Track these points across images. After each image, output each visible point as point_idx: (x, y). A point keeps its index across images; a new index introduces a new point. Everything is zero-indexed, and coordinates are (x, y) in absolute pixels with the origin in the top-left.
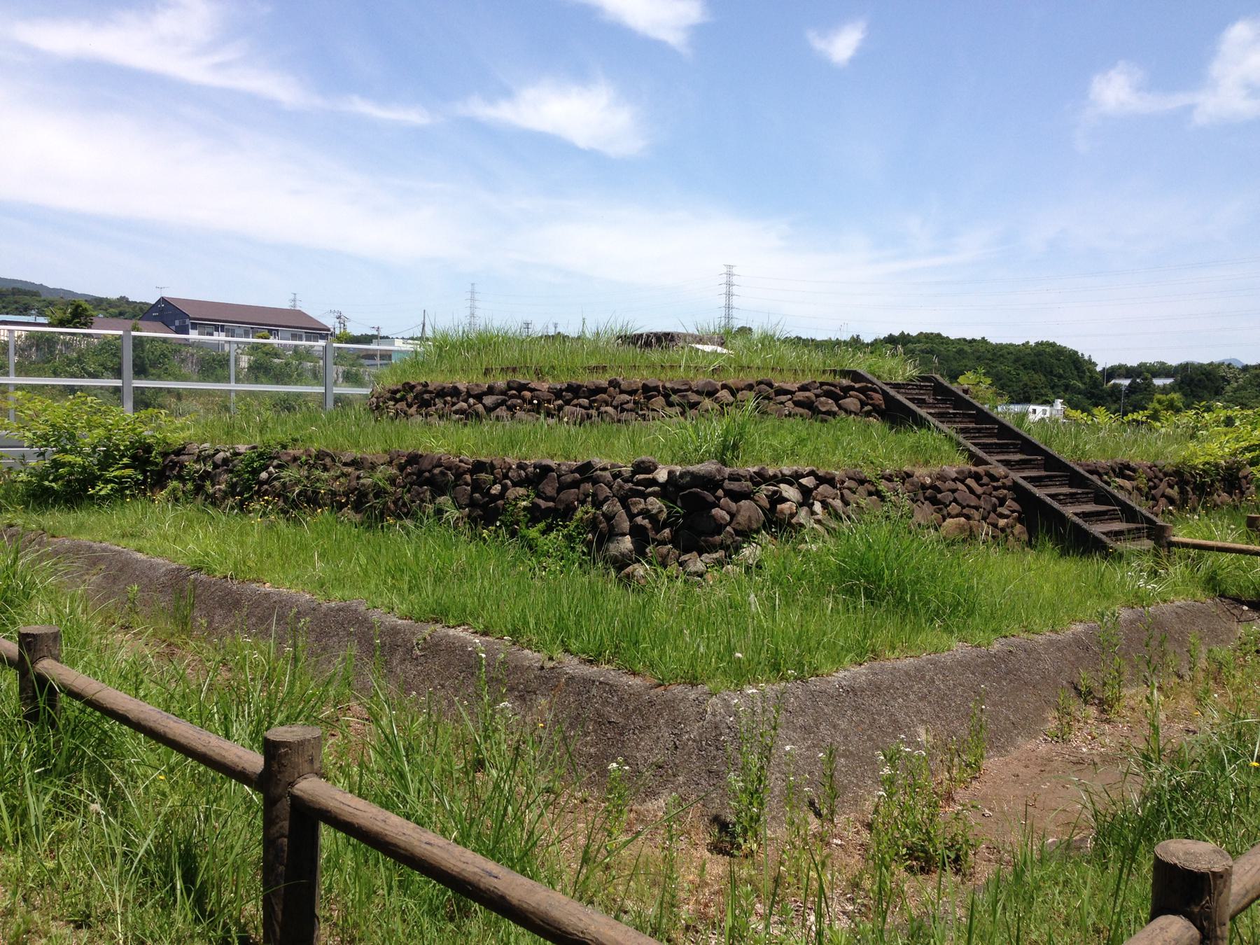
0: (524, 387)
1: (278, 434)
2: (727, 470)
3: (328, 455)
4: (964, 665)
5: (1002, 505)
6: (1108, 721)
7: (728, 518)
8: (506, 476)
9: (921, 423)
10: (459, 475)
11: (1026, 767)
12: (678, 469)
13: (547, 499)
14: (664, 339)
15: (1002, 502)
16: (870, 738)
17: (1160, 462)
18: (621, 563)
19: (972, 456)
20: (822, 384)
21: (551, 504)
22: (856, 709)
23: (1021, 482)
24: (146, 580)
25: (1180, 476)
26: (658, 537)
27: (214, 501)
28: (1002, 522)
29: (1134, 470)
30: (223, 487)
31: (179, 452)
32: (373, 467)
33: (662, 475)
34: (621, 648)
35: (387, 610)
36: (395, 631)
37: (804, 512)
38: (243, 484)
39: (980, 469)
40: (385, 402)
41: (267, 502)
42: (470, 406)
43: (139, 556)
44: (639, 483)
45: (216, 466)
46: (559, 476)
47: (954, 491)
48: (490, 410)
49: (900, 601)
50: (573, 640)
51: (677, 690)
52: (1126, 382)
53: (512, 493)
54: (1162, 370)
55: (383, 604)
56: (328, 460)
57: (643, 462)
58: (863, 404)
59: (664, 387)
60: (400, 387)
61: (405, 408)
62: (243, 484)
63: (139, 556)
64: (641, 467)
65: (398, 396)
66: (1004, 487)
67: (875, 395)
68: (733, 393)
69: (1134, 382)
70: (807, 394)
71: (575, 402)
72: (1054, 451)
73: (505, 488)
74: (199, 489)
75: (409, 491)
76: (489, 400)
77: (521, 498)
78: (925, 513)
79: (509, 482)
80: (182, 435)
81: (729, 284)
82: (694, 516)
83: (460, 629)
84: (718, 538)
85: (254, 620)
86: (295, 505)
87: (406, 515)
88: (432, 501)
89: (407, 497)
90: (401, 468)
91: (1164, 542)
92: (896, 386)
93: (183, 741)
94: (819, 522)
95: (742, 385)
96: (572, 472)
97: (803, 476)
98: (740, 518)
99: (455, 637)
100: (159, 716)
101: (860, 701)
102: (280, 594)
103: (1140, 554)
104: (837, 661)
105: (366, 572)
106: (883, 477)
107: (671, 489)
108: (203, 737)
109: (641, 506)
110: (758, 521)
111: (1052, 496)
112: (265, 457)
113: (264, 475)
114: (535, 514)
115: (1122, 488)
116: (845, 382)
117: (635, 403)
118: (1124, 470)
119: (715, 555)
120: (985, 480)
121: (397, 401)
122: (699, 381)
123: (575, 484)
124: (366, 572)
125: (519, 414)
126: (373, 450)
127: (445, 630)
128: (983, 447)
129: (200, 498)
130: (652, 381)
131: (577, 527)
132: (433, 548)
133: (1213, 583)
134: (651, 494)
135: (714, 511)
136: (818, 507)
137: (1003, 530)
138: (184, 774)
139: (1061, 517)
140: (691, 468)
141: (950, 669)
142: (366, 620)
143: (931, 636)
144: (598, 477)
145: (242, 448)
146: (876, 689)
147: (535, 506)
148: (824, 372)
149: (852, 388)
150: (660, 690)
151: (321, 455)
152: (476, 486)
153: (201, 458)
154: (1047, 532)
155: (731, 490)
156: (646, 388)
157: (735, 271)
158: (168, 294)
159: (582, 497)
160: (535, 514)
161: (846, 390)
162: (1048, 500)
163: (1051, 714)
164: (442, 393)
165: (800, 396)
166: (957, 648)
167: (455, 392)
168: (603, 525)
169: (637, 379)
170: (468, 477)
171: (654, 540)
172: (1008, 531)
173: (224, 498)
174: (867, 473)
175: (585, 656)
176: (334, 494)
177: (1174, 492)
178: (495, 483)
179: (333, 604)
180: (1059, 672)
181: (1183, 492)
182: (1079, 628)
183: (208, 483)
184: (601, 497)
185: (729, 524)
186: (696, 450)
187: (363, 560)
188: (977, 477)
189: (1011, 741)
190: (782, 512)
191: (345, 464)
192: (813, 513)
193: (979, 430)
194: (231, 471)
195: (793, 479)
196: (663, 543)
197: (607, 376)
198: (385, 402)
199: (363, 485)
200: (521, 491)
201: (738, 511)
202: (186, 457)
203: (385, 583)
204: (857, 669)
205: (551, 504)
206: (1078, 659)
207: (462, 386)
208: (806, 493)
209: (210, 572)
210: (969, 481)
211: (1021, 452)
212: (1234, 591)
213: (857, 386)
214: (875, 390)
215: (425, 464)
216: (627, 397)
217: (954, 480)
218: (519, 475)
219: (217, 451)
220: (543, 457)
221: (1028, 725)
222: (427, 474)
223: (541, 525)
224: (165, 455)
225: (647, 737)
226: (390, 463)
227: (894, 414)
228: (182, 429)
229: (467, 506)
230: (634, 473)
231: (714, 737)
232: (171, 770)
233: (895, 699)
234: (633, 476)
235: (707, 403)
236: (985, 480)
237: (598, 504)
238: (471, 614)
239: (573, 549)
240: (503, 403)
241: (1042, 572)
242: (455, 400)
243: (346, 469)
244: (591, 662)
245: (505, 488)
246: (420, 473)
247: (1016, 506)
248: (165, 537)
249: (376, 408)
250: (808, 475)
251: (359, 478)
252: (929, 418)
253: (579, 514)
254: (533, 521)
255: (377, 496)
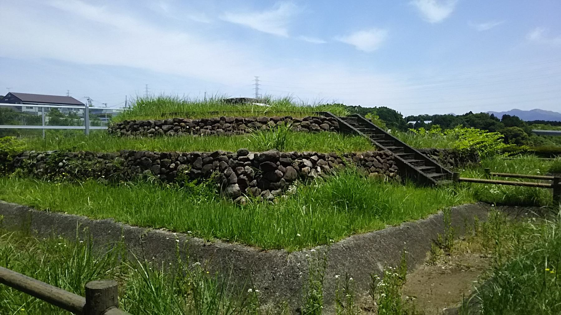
0: (182, 121)
1: (67, 145)
2: (281, 153)
3: (91, 153)
4: (391, 234)
5: (391, 167)
6: (449, 255)
7: (282, 174)
8: (177, 160)
9: (355, 133)
10: (154, 160)
11: (422, 277)
12: (259, 154)
13: (197, 169)
14: (242, 101)
15: (391, 165)
16: (359, 269)
17: (447, 148)
18: (234, 196)
19: (377, 147)
20: (313, 118)
21: (200, 171)
22: (351, 256)
23: (398, 157)
24: (7, 213)
25: (455, 154)
26: (251, 184)
27: (38, 176)
28: (392, 174)
29: (438, 152)
30: (42, 170)
31: (20, 155)
32: (113, 158)
33: (251, 156)
34: (244, 234)
35: (126, 222)
36: (129, 232)
37: (313, 170)
38: (50, 168)
39: (382, 152)
40: (115, 130)
41: (64, 176)
42: (156, 130)
43: (3, 202)
44: (241, 160)
45: (38, 161)
46: (203, 159)
47: (373, 161)
48: (165, 132)
49: (361, 207)
50: (218, 232)
51: (271, 252)
52: (414, 122)
53: (181, 167)
54: (427, 118)
55: (123, 219)
56: (91, 156)
57: (242, 151)
58: (330, 126)
59: (245, 120)
60: (122, 123)
61: (125, 132)
62: (50, 168)
63: (3, 202)
64: (241, 153)
65: (122, 127)
66: (391, 159)
67: (335, 122)
68: (276, 121)
69: (417, 122)
70: (307, 122)
71: (205, 127)
72: (407, 144)
73: (177, 165)
74: (30, 171)
75: (130, 168)
76: (165, 127)
77: (185, 169)
78: (362, 171)
79: (179, 162)
80: (22, 147)
81: (257, 85)
82: (268, 174)
83: (162, 229)
84: (278, 183)
85: (60, 229)
86: (76, 176)
87: (130, 179)
88: (142, 172)
89: (129, 171)
90: (126, 158)
91: (457, 180)
92: (343, 119)
93: (36, 290)
94: (320, 175)
95: (279, 118)
96: (209, 156)
97: (312, 155)
98: (287, 174)
99: (159, 233)
100: (21, 277)
101: (353, 253)
102: (72, 217)
103: (448, 186)
104: (340, 235)
105: (113, 205)
106: (344, 156)
107: (255, 163)
108: (48, 288)
109: (243, 170)
110: (295, 175)
111: (410, 163)
112: (61, 156)
113: (61, 164)
114: (192, 176)
115: (435, 159)
116: (322, 117)
117: (233, 127)
118: (434, 152)
119: (278, 191)
120: (384, 156)
121: (121, 129)
122: (260, 117)
123: (211, 162)
124: (113, 205)
125: (180, 133)
126: (112, 150)
127: (155, 230)
128: (380, 143)
129: (31, 175)
130: (239, 118)
131: (212, 181)
132: (146, 194)
133: (476, 196)
134: (246, 165)
135: (276, 171)
136: (319, 169)
137: (392, 177)
138: (34, 307)
139: (416, 171)
140: (265, 153)
141: (386, 236)
142: (115, 227)
143: (377, 222)
144: (222, 158)
145: (50, 152)
146: (358, 247)
147: (192, 172)
148: (313, 113)
149: (326, 119)
150: (263, 253)
151: (87, 154)
152: (163, 165)
153: (30, 158)
154: (410, 177)
155: (283, 162)
156: (237, 121)
157: (259, 79)
158: (12, 91)
159: (214, 167)
160: (192, 176)
161: (323, 120)
162: (409, 164)
163: (428, 253)
164: (142, 125)
165: (304, 123)
166: (388, 228)
167: (149, 124)
168: (225, 180)
169: (233, 117)
170: (159, 161)
171: (249, 185)
172: (394, 178)
173: (42, 175)
174: (338, 154)
175: (224, 239)
176: (94, 171)
177: (452, 161)
178: (172, 163)
179: (98, 221)
180: (427, 235)
181: (455, 161)
182: (431, 216)
183: (35, 168)
184: (223, 167)
185: (283, 177)
186: (265, 145)
187: (112, 199)
188: (381, 155)
189: (414, 266)
190: (304, 171)
191: (99, 157)
192: (317, 172)
193: (377, 137)
194: (45, 163)
195: (308, 157)
196: (254, 186)
197: (219, 115)
198: (115, 130)
199: (108, 166)
200: (185, 166)
201: (286, 171)
202: (24, 157)
203: (123, 210)
204: (349, 238)
205: (200, 171)
206: (433, 229)
207: (152, 121)
208: (314, 163)
209: (39, 208)
210: (377, 157)
211: (395, 145)
212: (485, 199)
213: (327, 118)
214: (335, 120)
215: (138, 156)
216: (229, 125)
217: (372, 157)
218: (184, 159)
219: (39, 154)
220: (194, 151)
221: (419, 259)
222: (139, 160)
223: (195, 181)
224: (14, 157)
225: (259, 275)
226: (121, 156)
227: (343, 129)
228: (22, 145)
229: (159, 174)
230: (238, 156)
231: (293, 273)
232: (28, 304)
233: (367, 251)
234: (238, 157)
235: (264, 126)
236: (384, 156)
237: (222, 171)
238: (167, 222)
239: (212, 191)
240: (172, 128)
241: (407, 195)
242: (149, 127)
243: (99, 160)
244: (228, 241)
245: (177, 165)
246: (135, 160)
247: (396, 167)
248: (16, 193)
249: (112, 132)
250: (314, 155)
251: (106, 163)
252: (358, 131)
253: (213, 175)
254: (192, 179)
255: (115, 171)
